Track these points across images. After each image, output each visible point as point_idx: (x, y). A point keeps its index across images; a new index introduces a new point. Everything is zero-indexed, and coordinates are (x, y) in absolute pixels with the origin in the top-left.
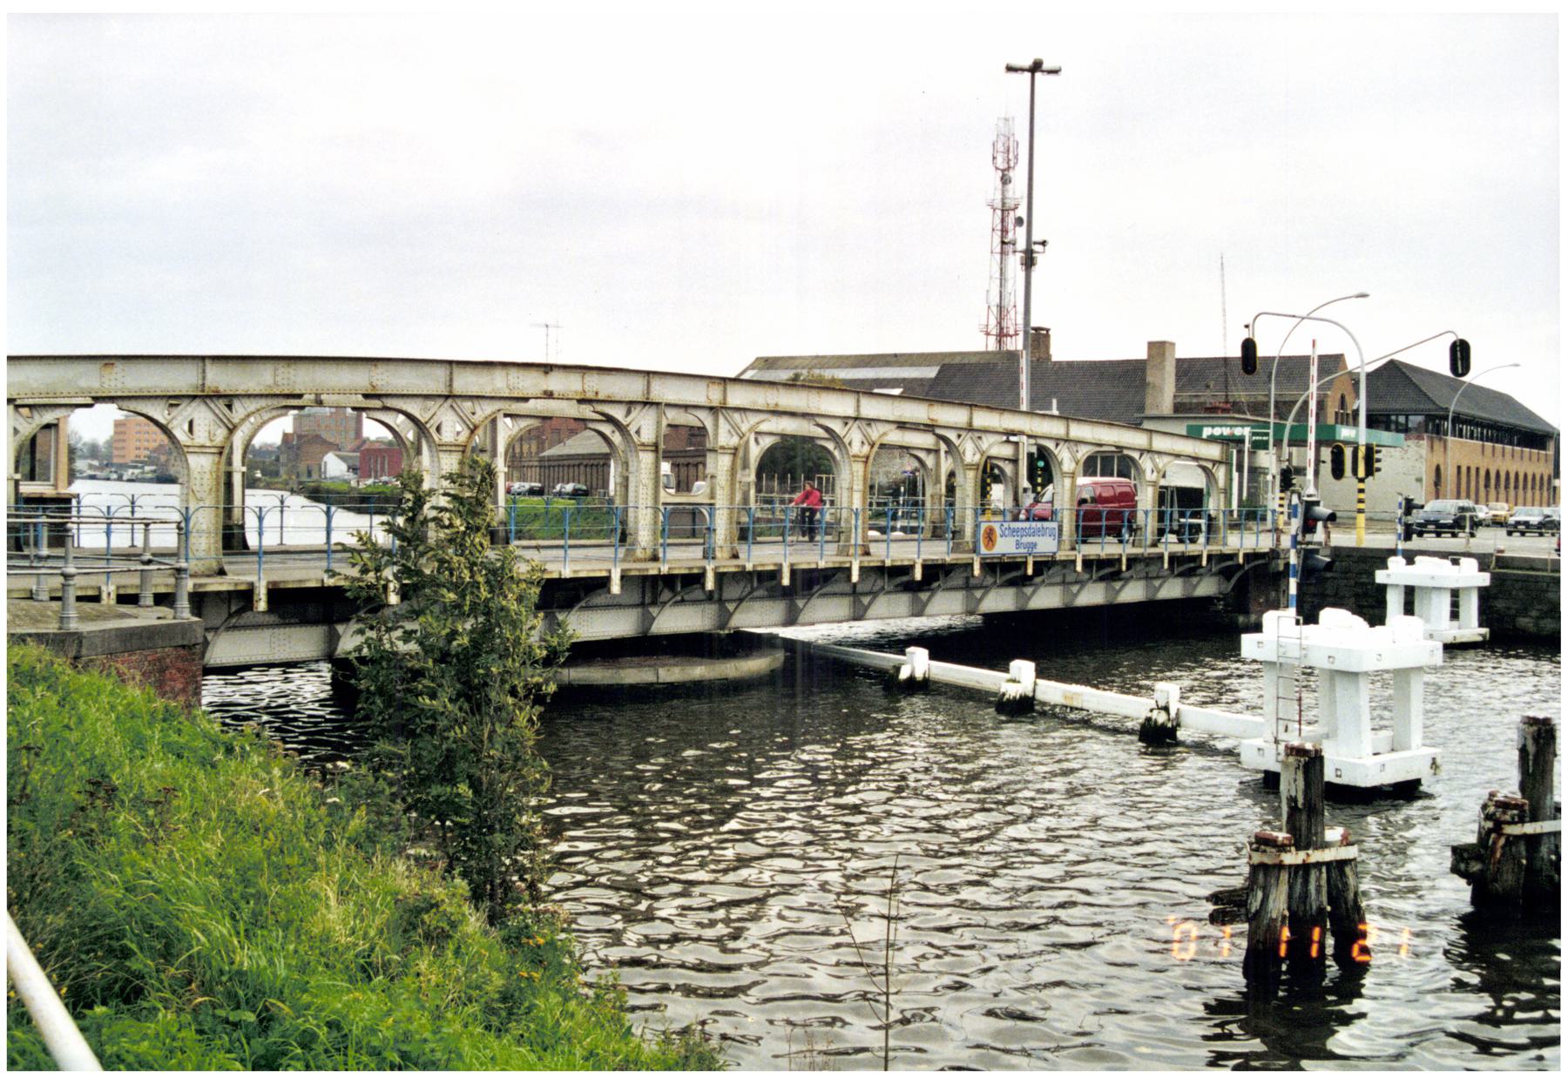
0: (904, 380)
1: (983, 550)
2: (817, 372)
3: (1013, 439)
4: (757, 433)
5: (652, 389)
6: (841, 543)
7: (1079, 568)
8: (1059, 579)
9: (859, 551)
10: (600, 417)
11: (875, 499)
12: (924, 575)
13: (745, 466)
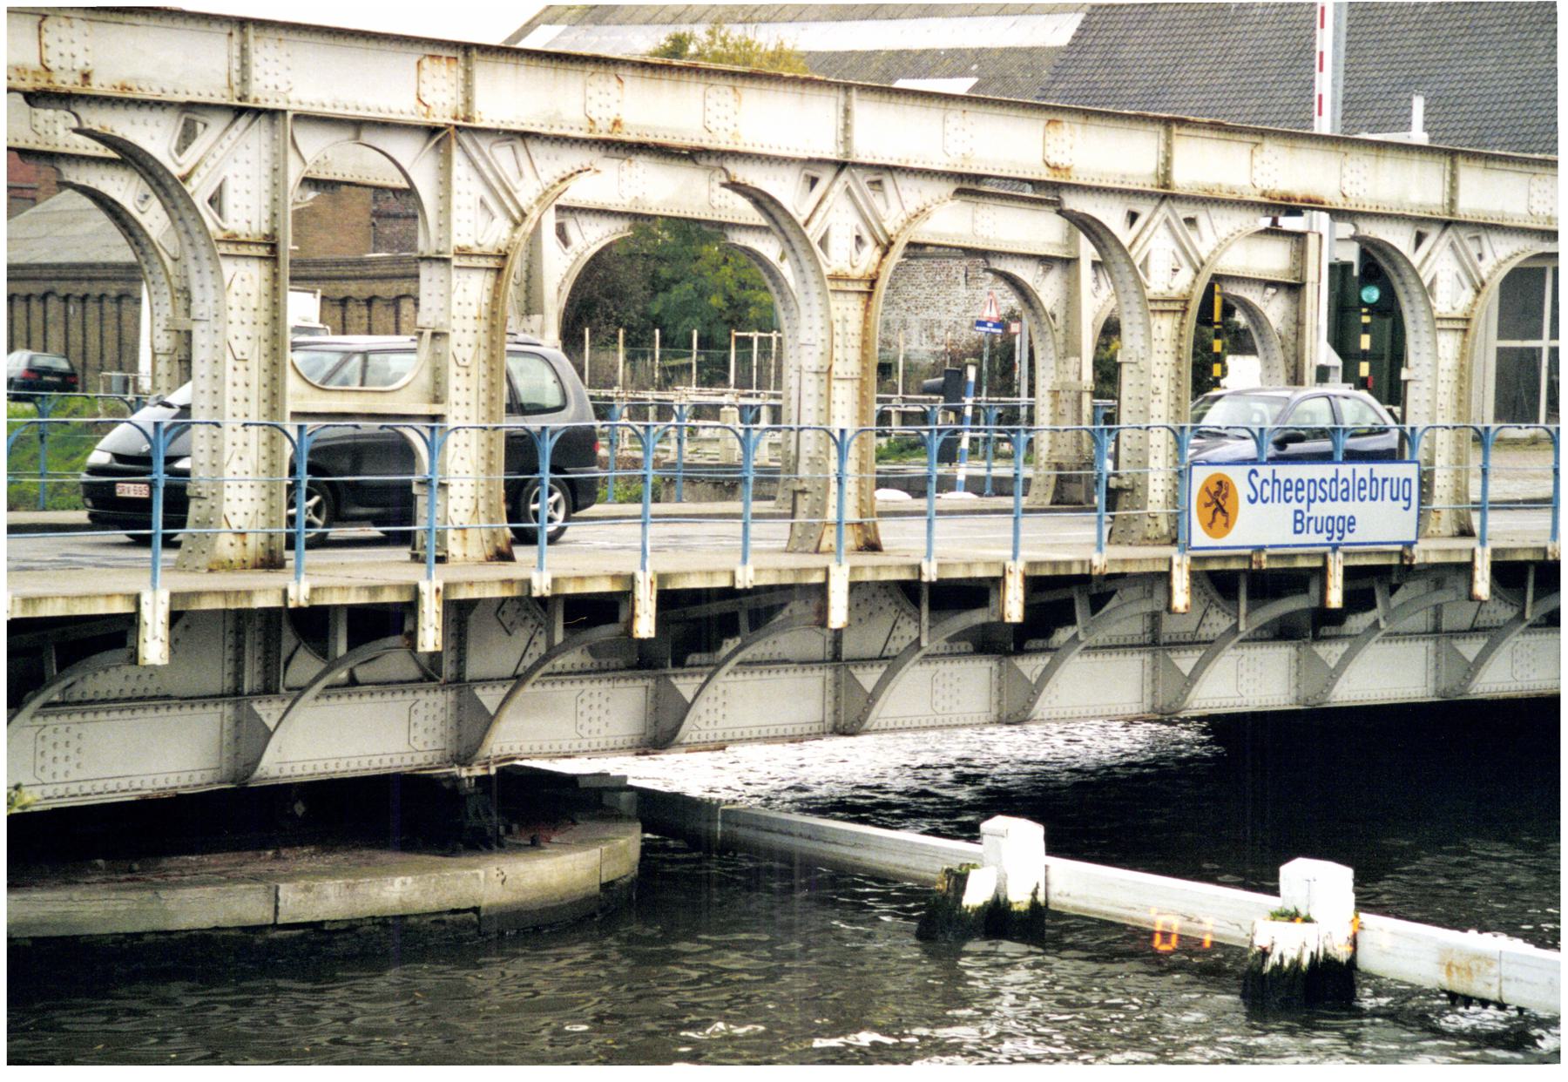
0: (979, 54)
1: (1200, 537)
2: (736, 32)
3: (1288, 223)
4: (560, 208)
5: (255, 72)
6: (801, 519)
7: (1482, 586)
8: (1421, 620)
9: (850, 539)
10: (111, 154)
11: (896, 406)
12: (1028, 607)
13: (531, 306)
